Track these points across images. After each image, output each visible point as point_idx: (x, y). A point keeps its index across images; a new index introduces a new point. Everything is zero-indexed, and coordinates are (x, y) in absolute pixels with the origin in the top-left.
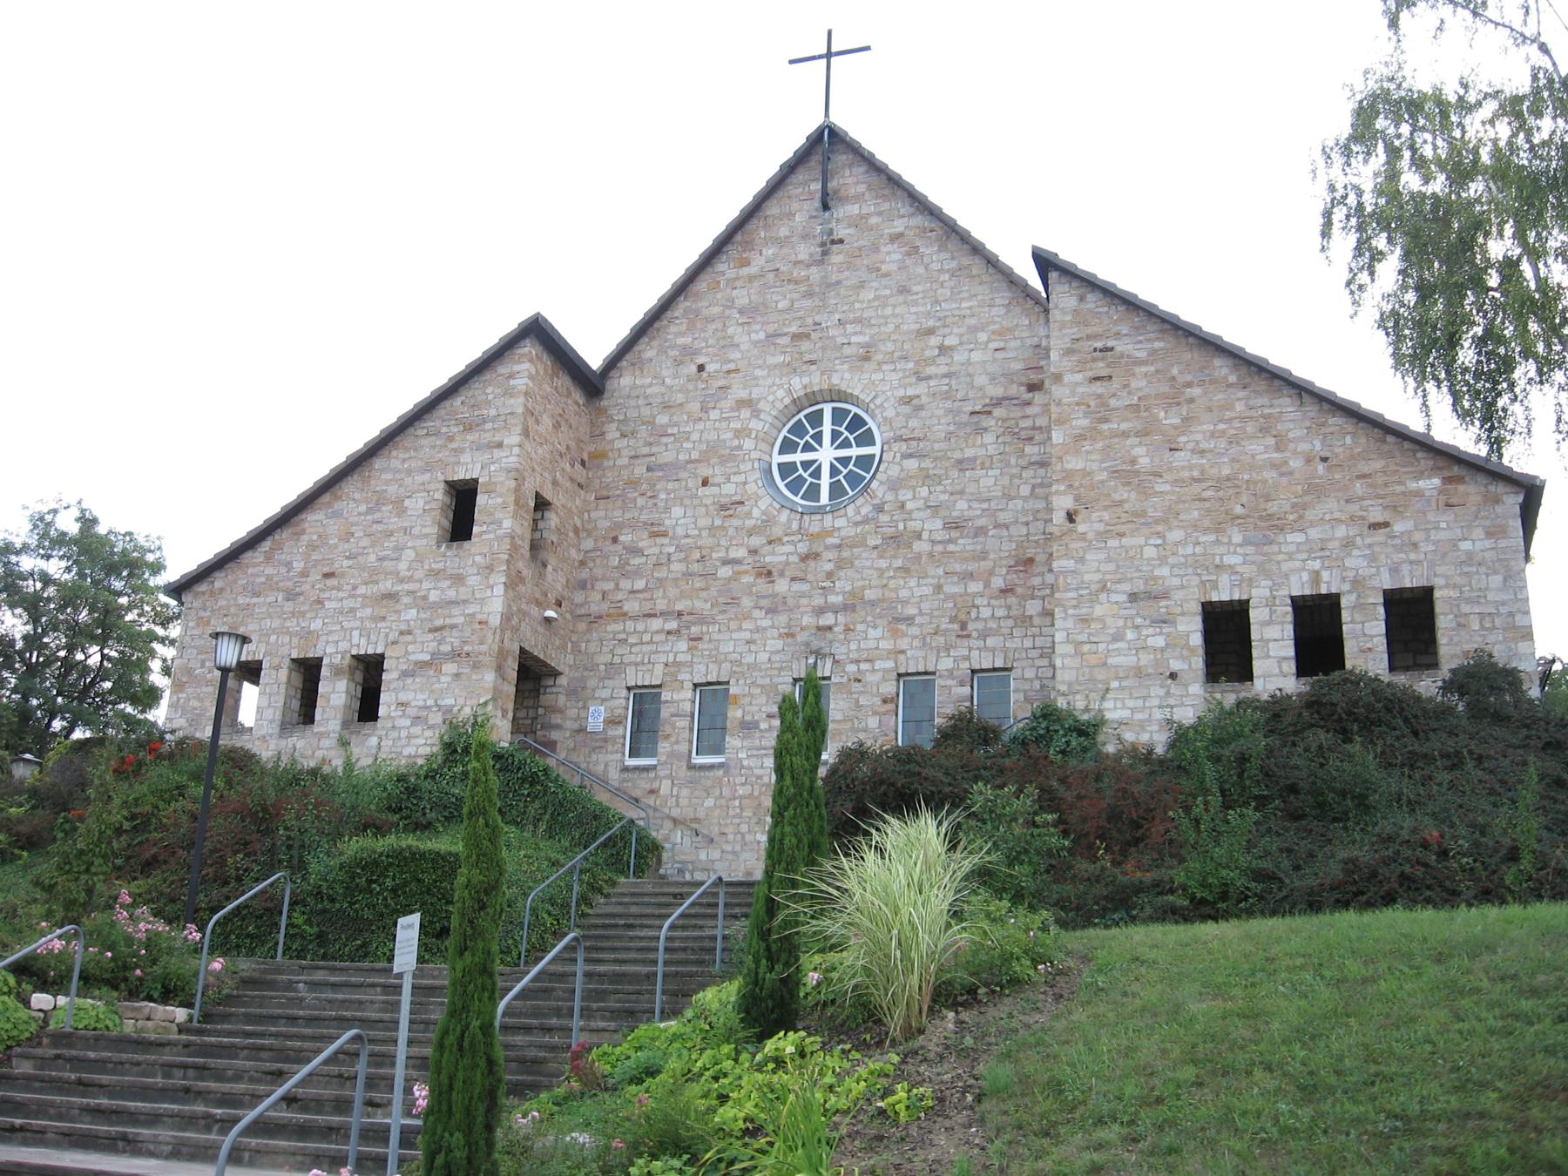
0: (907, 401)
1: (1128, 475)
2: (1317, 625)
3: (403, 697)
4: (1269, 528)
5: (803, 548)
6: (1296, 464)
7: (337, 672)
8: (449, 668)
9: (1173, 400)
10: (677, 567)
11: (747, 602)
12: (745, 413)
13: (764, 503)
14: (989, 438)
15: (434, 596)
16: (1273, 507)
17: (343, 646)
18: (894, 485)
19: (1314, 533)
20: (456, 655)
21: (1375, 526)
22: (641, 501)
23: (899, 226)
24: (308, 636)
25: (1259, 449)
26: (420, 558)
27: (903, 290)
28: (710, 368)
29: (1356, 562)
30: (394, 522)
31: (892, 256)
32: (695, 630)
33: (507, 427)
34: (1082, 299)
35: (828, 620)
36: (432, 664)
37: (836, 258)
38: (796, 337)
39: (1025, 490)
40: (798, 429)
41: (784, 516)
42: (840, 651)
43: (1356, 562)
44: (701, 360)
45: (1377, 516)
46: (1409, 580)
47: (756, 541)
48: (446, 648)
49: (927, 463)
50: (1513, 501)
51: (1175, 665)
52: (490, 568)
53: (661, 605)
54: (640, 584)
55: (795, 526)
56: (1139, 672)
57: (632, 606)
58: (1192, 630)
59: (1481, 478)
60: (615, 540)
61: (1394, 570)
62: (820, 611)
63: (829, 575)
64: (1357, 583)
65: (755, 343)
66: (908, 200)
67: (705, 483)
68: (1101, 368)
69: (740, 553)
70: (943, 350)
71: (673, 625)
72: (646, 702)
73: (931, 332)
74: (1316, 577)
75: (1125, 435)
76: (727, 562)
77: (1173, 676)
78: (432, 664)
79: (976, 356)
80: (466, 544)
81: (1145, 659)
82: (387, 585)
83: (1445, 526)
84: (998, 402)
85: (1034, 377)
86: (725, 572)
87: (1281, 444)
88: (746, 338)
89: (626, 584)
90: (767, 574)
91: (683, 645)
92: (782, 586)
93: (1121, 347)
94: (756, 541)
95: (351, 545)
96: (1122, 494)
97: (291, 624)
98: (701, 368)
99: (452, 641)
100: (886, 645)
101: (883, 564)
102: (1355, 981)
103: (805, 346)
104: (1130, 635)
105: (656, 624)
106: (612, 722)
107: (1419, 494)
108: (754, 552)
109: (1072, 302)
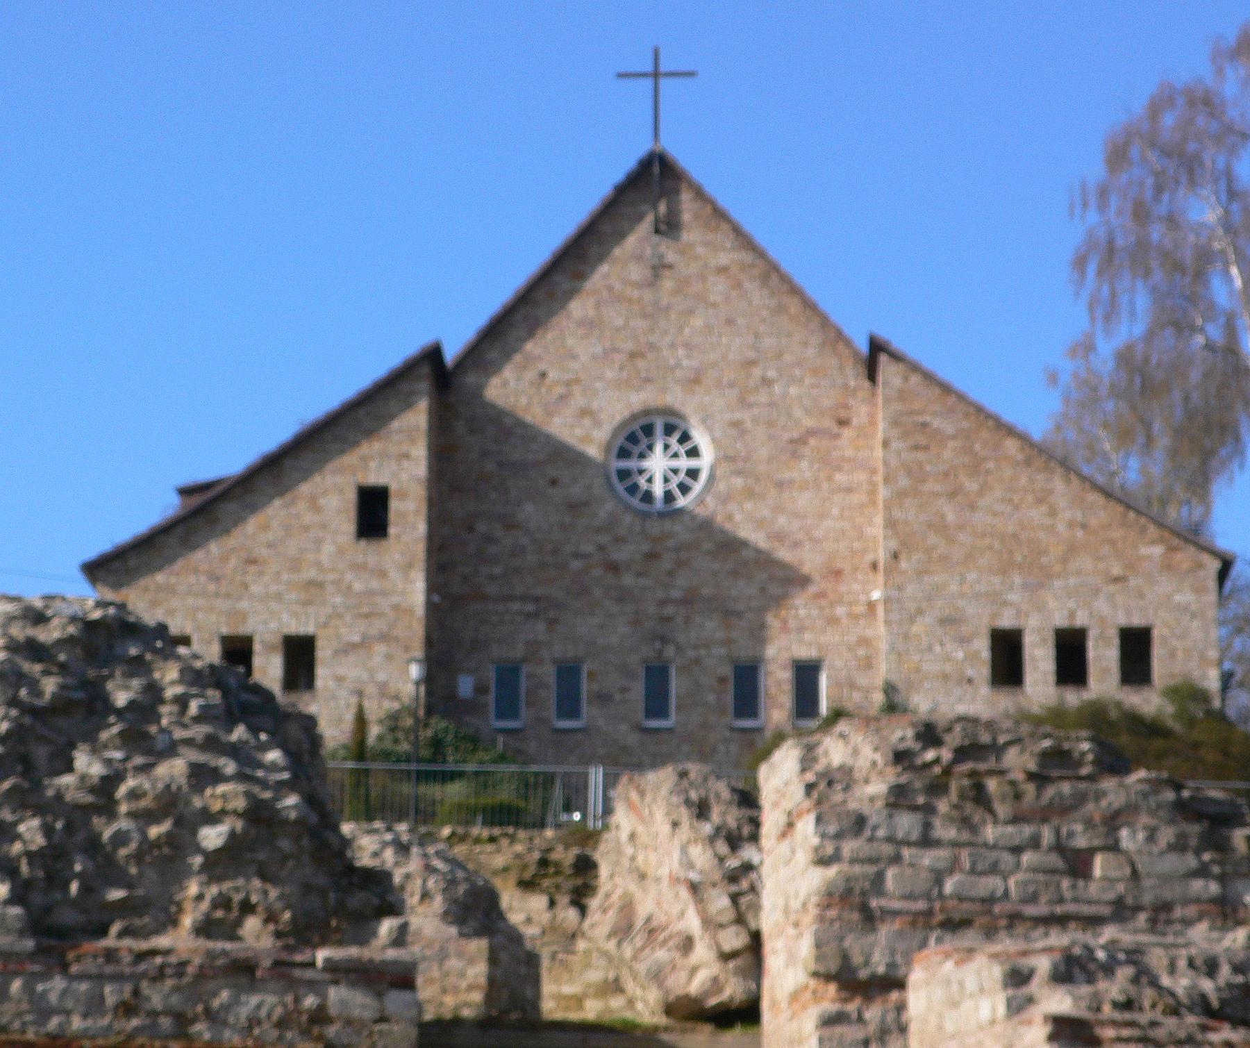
0: (736, 424)
1: (940, 527)
2: (1071, 655)
3: (340, 671)
4: (1039, 577)
5: (646, 547)
6: (1061, 528)
7: (269, 648)
8: (380, 649)
9: (975, 469)
10: (531, 558)
11: (598, 592)
12: (587, 422)
13: (609, 506)
14: (804, 464)
15: (358, 586)
16: (1044, 560)
17: (273, 625)
18: (725, 499)
19: (1072, 581)
20: (384, 638)
21: (1117, 580)
22: (493, 495)
23: (724, 259)
24: (244, 617)
25: (1036, 515)
26: (341, 552)
27: (730, 322)
28: (553, 375)
29: (1102, 605)
30: (308, 518)
31: (718, 288)
32: (552, 614)
33: (413, 441)
34: (906, 379)
35: (669, 610)
36: (364, 645)
37: (668, 284)
38: (633, 356)
39: (835, 511)
40: (632, 439)
41: (628, 519)
42: (682, 638)
43: (1102, 605)
44: (542, 366)
45: (1116, 571)
46: (1137, 621)
47: (603, 539)
48: (373, 632)
49: (751, 481)
50: (1214, 565)
51: (970, 672)
52: (410, 566)
53: (519, 590)
54: (497, 570)
55: (638, 528)
56: (946, 677)
57: (492, 589)
58: (983, 647)
59: (1192, 549)
60: (471, 529)
61: (1128, 612)
62: (663, 603)
63: (670, 573)
64: (1102, 621)
65: (594, 357)
66: (732, 236)
67: (554, 482)
68: (921, 439)
69: (589, 548)
70: (767, 382)
71: (530, 607)
72: (508, 675)
73: (752, 363)
74: (1072, 615)
75: (936, 495)
76: (577, 555)
77: (970, 681)
78: (364, 645)
79: (793, 390)
80: (384, 544)
81: (948, 668)
82: (313, 574)
83: (1164, 585)
84: (811, 433)
85: (843, 414)
86: (576, 564)
87: (1053, 513)
88: (586, 349)
89: (485, 570)
90: (614, 568)
91: (541, 627)
92: (628, 580)
93: (936, 423)
94: (603, 539)
95: (270, 536)
96: (932, 539)
97: (220, 604)
98: (543, 375)
99: (379, 626)
100: (720, 635)
101: (716, 566)
102: (1145, 795)
103: (641, 364)
104: (938, 648)
105: (516, 606)
106: (481, 689)
107: (1149, 558)
108: (601, 548)
109: (897, 382)
